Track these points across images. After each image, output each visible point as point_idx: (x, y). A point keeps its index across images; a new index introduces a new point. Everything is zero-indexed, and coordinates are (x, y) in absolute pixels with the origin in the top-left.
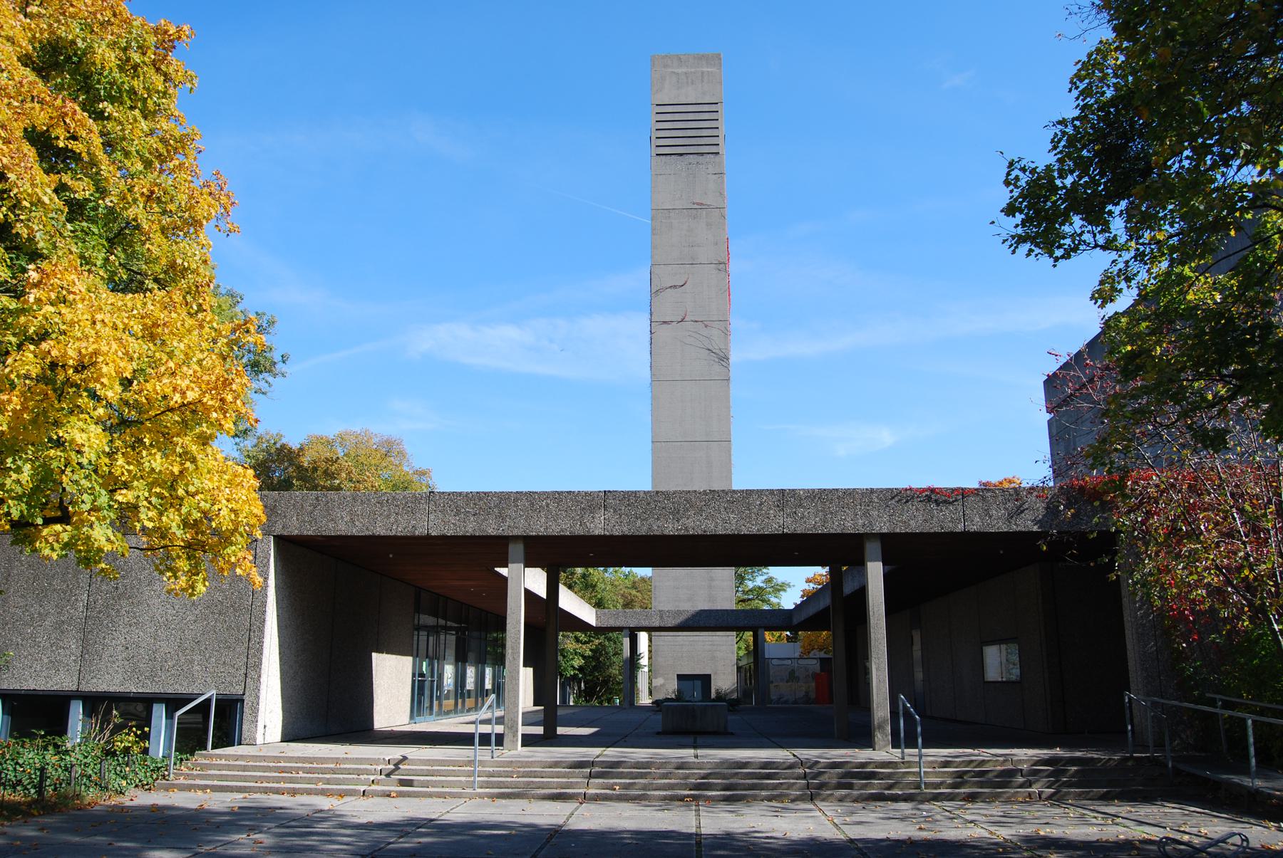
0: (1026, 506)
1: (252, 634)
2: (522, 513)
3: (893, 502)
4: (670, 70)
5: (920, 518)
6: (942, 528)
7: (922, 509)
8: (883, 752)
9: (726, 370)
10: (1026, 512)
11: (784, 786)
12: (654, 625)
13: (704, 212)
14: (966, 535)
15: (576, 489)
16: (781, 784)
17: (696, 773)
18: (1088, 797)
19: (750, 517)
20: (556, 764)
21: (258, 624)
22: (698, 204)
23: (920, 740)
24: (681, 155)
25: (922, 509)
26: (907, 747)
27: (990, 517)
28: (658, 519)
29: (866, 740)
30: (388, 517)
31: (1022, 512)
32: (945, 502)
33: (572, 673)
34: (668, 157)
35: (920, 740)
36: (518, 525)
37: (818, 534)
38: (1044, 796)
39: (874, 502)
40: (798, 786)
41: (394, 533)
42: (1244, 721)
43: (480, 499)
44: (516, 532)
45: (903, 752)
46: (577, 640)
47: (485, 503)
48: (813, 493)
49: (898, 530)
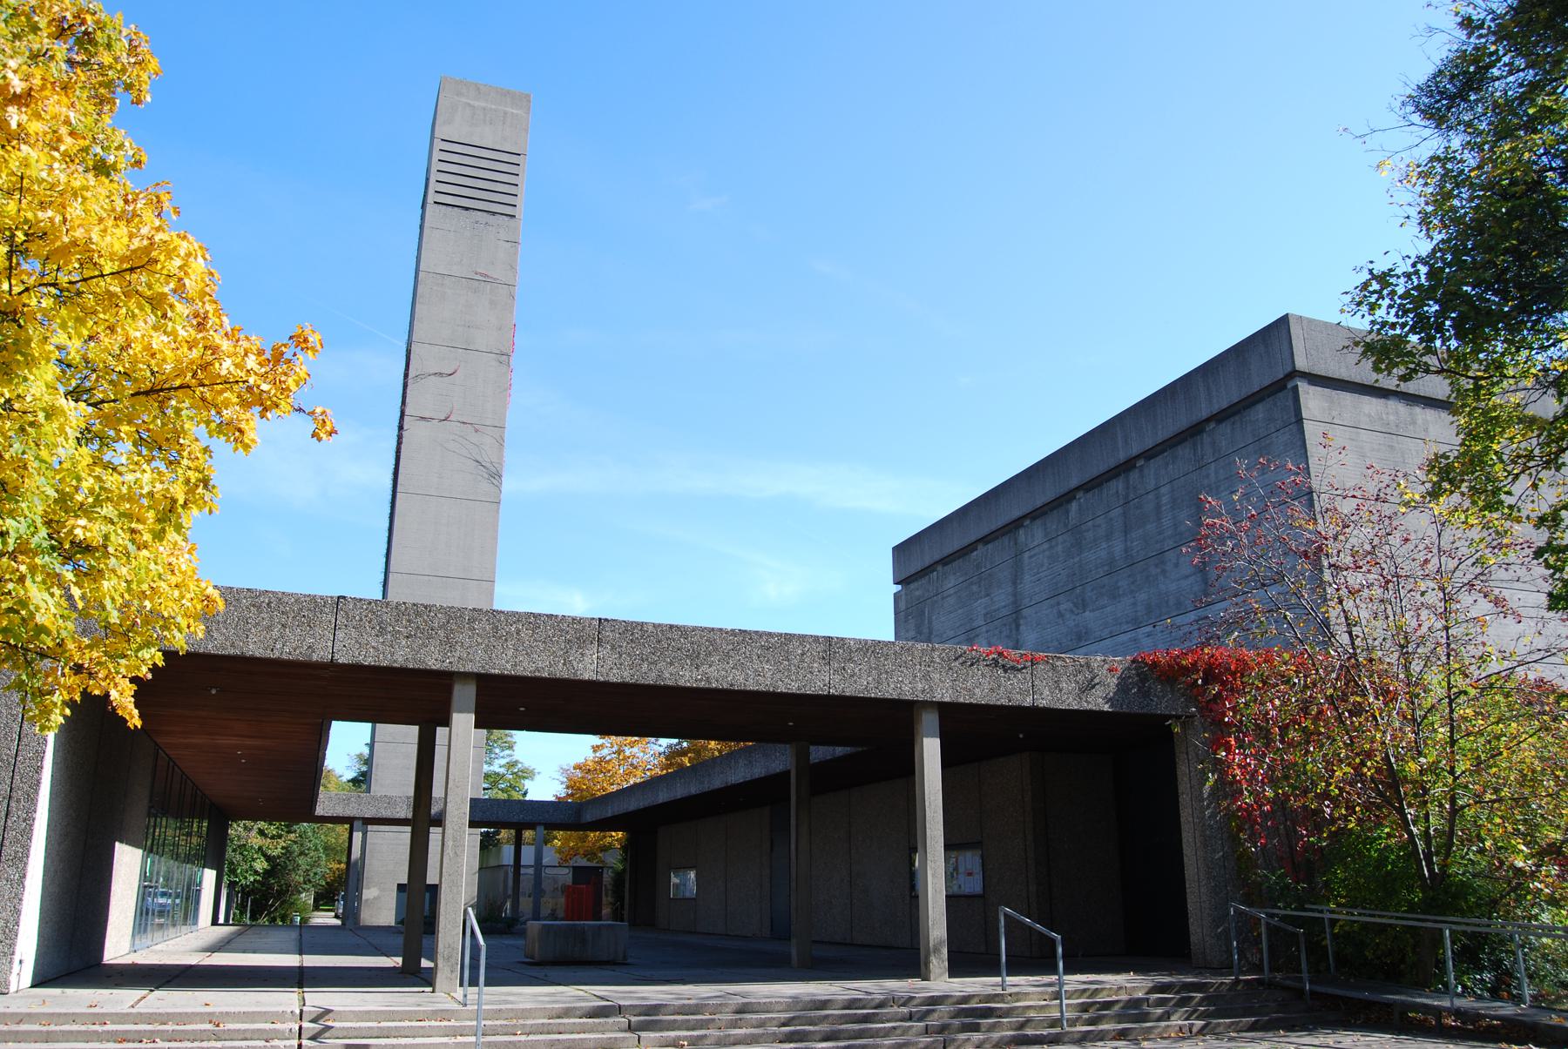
0: (1097, 680)
1: (13, 804)
2: (480, 640)
3: (957, 663)
4: (464, 100)
5: (986, 686)
6: (1010, 701)
7: (988, 675)
8: (941, 983)
9: (497, 491)
10: (1097, 687)
11: (898, 1032)
12: (397, 816)
13: (488, 286)
14: (1034, 711)
15: (560, 613)
16: (894, 1028)
17: (774, 1019)
18: (1238, 1029)
19: (789, 670)
20: (567, 1013)
21: (26, 787)
22: (482, 275)
23: (1061, 965)
24: (467, 209)
25: (988, 675)
26: (1008, 975)
27: (1060, 690)
28: (671, 664)
29: (910, 963)
30: (269, 628)
31: (1093, 687)
32: (1013, 668)
33: (252, 879)
34: (450, 208)
35: (1061, 965)
36: (473, 657)
37: (871, 698)
38: (1195, 1030)
39: (934, 662)
40: (914, 1029)
41: (276, 655)
42: (1441, 931)
43: (418, 614)
44: (469, 668)
45: (1003, 981)
46: (261, 832)
47: (425, 621)
48: (866, 644)
49: (962, 700)
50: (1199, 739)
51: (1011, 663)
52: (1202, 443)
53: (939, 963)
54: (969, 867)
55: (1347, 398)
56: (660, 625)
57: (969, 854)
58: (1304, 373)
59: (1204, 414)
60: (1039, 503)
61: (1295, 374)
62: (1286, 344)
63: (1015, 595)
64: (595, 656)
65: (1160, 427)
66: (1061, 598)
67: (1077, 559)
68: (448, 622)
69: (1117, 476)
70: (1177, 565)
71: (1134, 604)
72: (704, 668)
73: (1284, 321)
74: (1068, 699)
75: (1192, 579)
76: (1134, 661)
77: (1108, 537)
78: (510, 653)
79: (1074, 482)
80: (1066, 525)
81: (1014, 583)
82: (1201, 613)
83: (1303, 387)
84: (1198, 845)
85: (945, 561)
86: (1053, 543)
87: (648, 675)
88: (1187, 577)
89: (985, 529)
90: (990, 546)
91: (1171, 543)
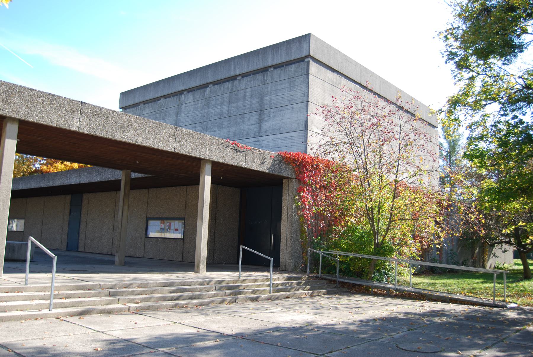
0: (266, 160)
3: (221, 146)
8: (203, 274)
19: (160, 139)
27: (254, 162)
28: (112, 128)
31: (265, 162)
50: (293, 185)
51: (240, 149)
52: (267, 75)
53: (203, 266)
54: (176, 227)
55: (323, 70)
56: (108, 110)
57: (177, 222)
58: (312, 57)
59: (270, 64)
60: (192, 86)
61: (309, 56)
62: (307, 45)
63: (176, 121)
64: (78, 120)
65: (250, 65)
66: (197, 125)
67: (206, 111)
68: (8, 91)
69: (228, 81)
70: (249, 120)
71: (229, 132)
72: (126, 133)
73: (308, 36)
74: (256, 167)
75: (254, 126)
76: (278, 154)
77: (221, 104)
78: (39, 111)
79: (210, 80)
80: (203, 97)
81: (177, 116)
82: (256, 139)
83: (311, 62)
84: (288, 226)
85: (145, 102)
86: (197, 103)
87: (101, 132)
88: (253, 125)
89: (166, 92)
90: (167, 99)
91: (248, 111)
